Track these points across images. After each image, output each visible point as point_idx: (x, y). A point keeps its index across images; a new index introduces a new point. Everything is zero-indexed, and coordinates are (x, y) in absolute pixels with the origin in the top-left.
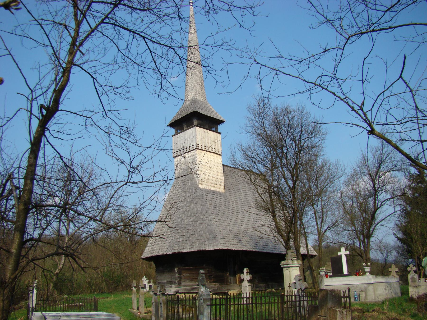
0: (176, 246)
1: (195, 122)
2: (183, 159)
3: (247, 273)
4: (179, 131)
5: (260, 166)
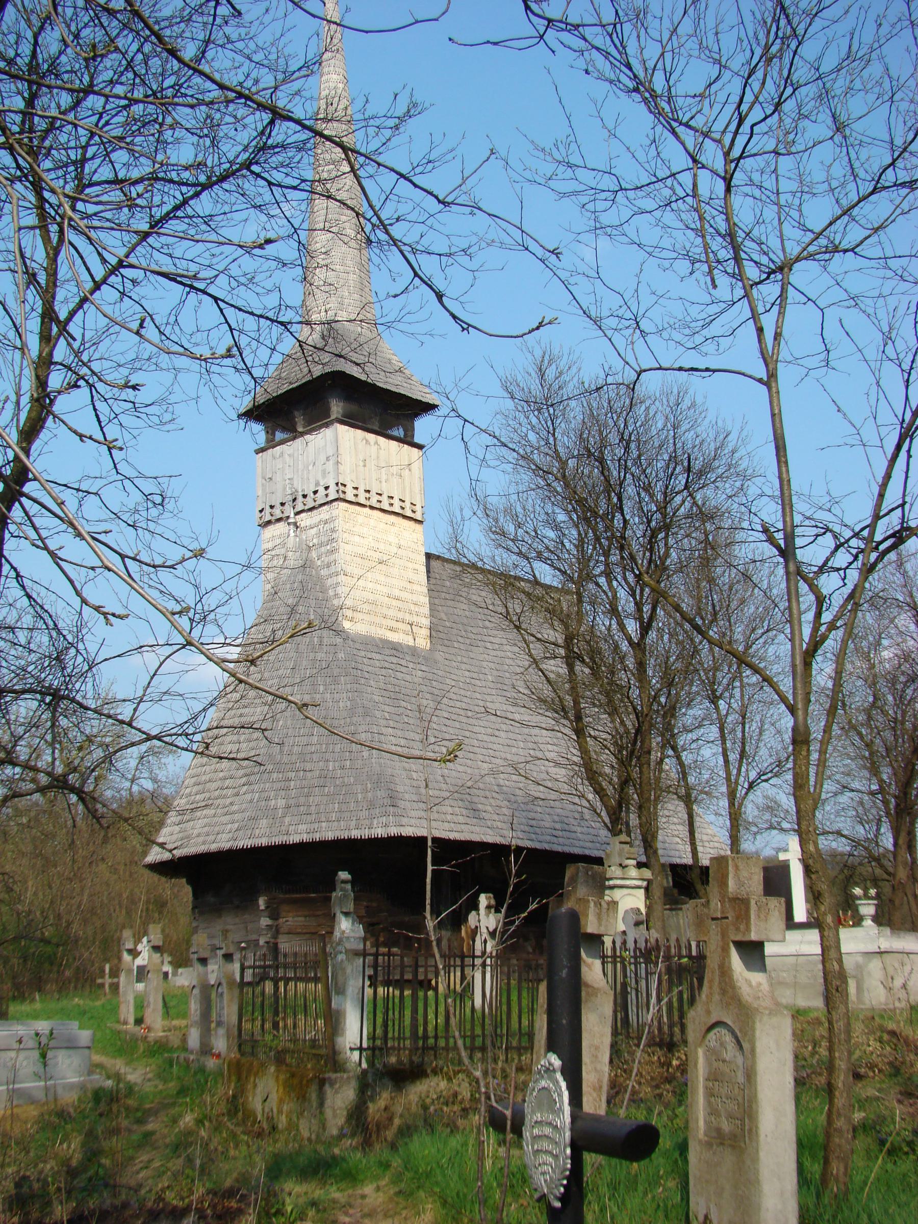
0: (264, 822)
1: (337, 408)
2: (292, 534)
3: (488, 907)
4: (279, 435)
5: (539, 566)
